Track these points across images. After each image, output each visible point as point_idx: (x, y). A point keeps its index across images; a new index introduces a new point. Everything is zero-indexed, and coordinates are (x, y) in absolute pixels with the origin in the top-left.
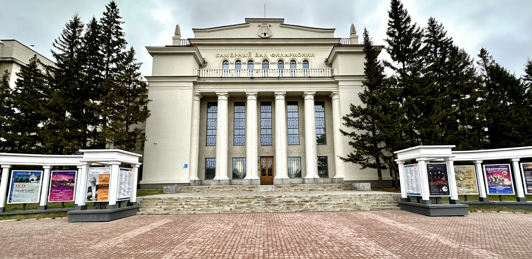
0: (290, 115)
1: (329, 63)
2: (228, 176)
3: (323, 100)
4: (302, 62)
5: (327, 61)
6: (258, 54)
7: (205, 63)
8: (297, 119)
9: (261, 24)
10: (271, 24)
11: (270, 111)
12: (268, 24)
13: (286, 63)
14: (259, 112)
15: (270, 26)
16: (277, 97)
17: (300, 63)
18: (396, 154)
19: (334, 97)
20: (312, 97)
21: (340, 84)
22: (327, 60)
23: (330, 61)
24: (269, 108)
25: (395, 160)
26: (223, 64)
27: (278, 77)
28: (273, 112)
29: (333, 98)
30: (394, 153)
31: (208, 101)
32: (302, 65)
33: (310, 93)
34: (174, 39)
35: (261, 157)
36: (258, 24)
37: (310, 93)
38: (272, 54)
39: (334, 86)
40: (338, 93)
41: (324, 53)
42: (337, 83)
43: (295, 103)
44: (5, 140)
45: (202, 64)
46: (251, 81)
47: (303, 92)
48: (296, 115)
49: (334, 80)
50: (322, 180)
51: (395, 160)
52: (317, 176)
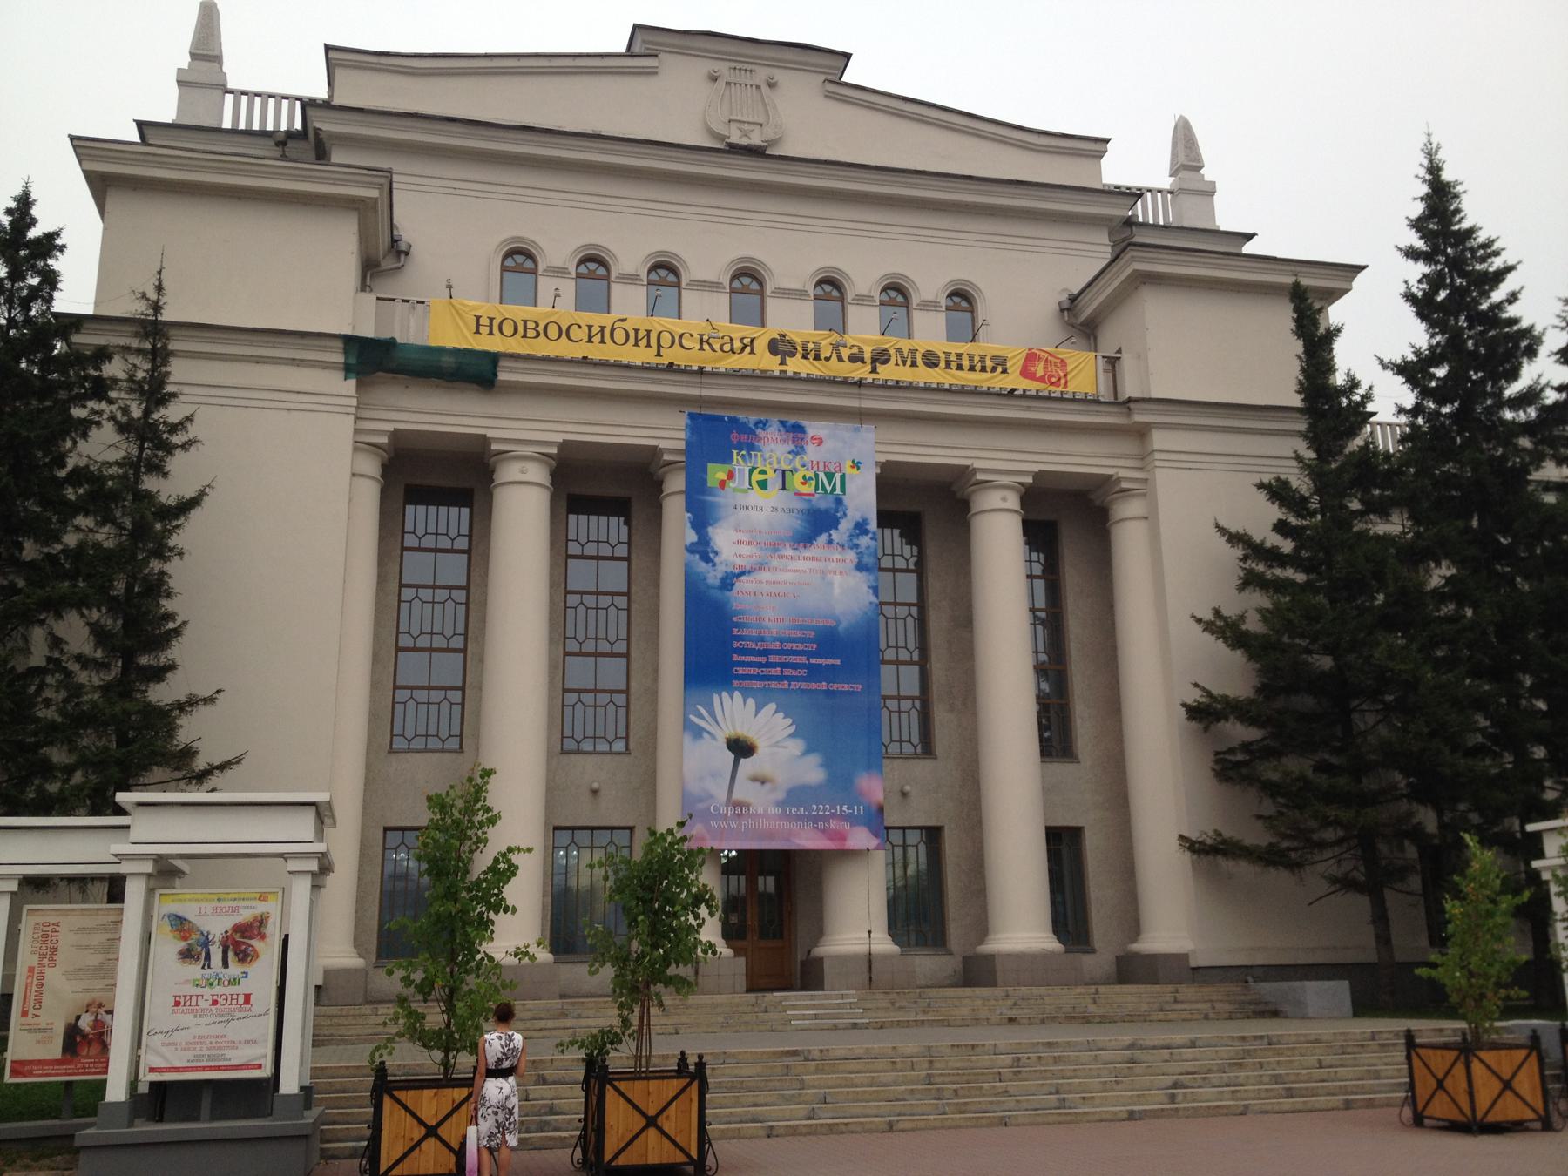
0: (581, 575)
1: (1082, 320)
2: (358, 943)
3: (1068, 522)
4: (943, 302)
5: (1070, 306)
6: (708, 240)
7: (398, 250)
8: (622, 602)
9: (723, 68)
10: (779, 75)
11: (622, 551)
12: (762, 74)
13: (861, 300)
14: (561, 552)
15: (772, 85)
16: (509, 472)
17: (559, 272)
18: (1538, 836)
19: (1127, 509)
20: (1013, 501)
21: (1159, 440)
22: (1073, 299)
23: (1088, 309)
24: (456, 518)
25: (1535, 864)
26: (504, 269)
27: (701, 371)
28: (477, 548)
29: (975, 508)
30: (1530, 827)
31: (433, 483)
32: (723, 300)
33: (1006, 480)
34: (184, 82)
35: (556, 828)
36: (733, 65)
37: (1006, 480)
38: (794, 248)
39: (1128, 446)
40: (1144, 489)
41: (1077, 262)
42: (1141, 433)
43: (618, 507)
44: (1467, 837)
45: (382, 259)
46: (695, 391)
47: (964, 473)
48: (614, 576)
49: (1128, 417)
50: (926, 963)
51: (1535, 864)
52: (883, 944)
